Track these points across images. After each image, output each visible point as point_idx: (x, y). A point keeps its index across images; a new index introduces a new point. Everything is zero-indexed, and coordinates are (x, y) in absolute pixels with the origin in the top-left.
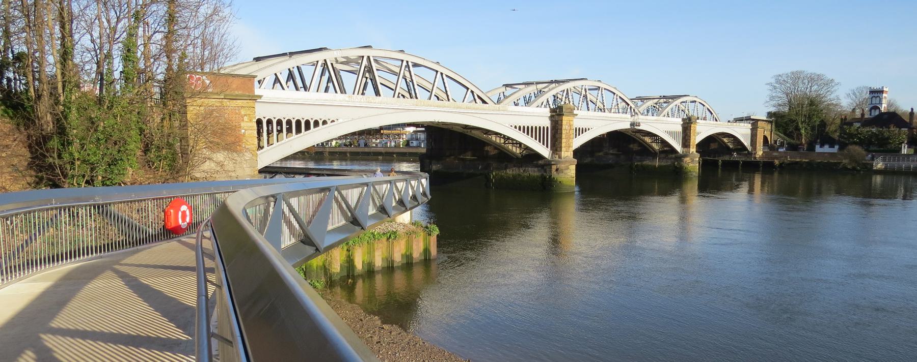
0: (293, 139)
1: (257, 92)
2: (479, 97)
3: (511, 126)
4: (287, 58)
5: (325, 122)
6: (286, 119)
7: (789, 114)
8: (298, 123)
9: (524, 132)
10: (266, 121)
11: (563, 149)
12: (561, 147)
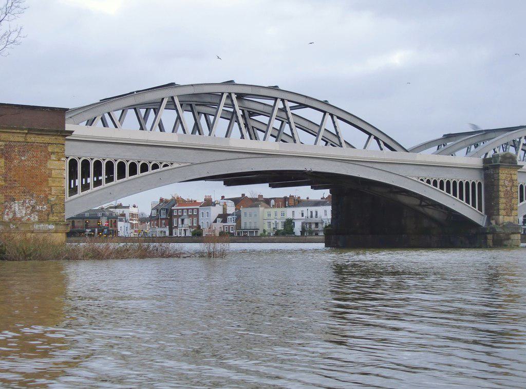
0: (114, 185)
1: (68, 127)
2: (386, 145)
3: (422, 180)
4: (337, 128)
5: (155, 167)
6: (106, 161)
7: (485, 229)
8: (121, 166)
9: (448, 191)
10: (105, 163)
11: (502, 212)
12: (498, 210)
